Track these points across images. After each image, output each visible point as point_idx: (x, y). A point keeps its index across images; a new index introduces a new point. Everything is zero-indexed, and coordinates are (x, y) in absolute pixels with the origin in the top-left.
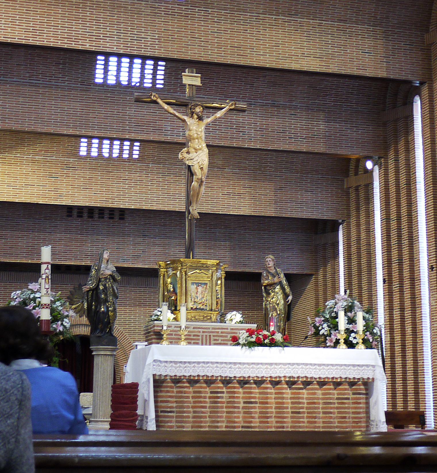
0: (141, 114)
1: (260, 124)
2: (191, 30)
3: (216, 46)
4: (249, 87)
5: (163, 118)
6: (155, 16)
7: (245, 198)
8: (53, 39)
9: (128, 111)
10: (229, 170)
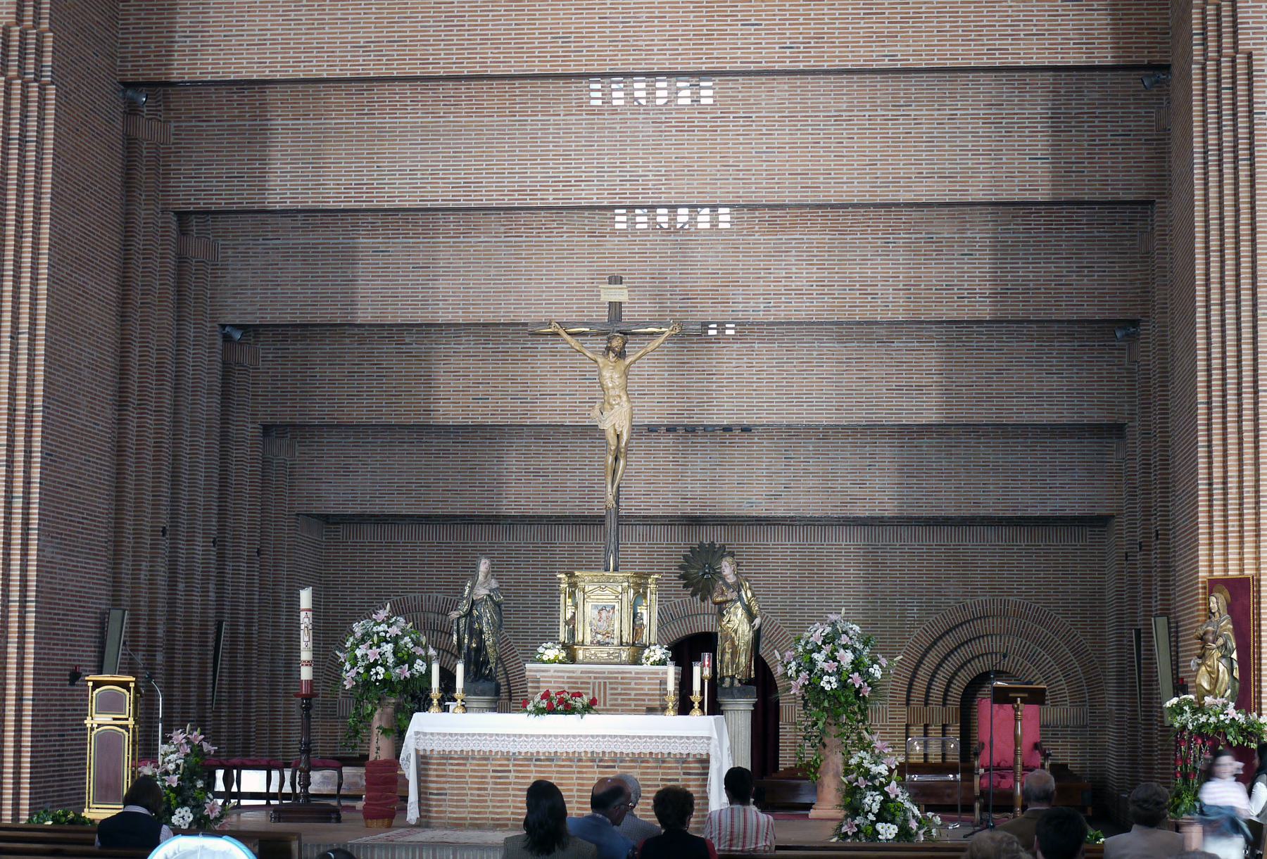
0: (691, 278)
1: (903, 277)
2: (720, 153)
3: (764, 176)
4: (883, 213)
5: (730, 282)
6: (661, 136)
7: (929, 394)
8: (497, 195)
9: (669, 274)
10: (901, 345)
